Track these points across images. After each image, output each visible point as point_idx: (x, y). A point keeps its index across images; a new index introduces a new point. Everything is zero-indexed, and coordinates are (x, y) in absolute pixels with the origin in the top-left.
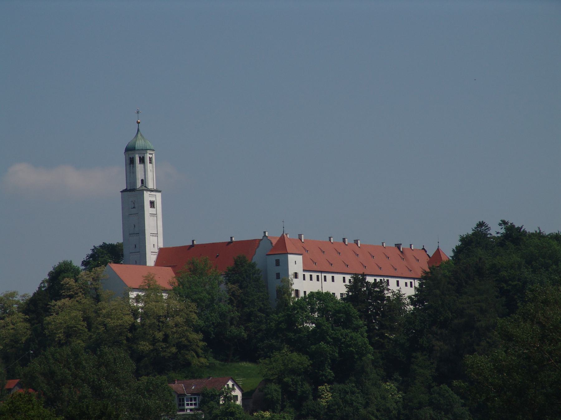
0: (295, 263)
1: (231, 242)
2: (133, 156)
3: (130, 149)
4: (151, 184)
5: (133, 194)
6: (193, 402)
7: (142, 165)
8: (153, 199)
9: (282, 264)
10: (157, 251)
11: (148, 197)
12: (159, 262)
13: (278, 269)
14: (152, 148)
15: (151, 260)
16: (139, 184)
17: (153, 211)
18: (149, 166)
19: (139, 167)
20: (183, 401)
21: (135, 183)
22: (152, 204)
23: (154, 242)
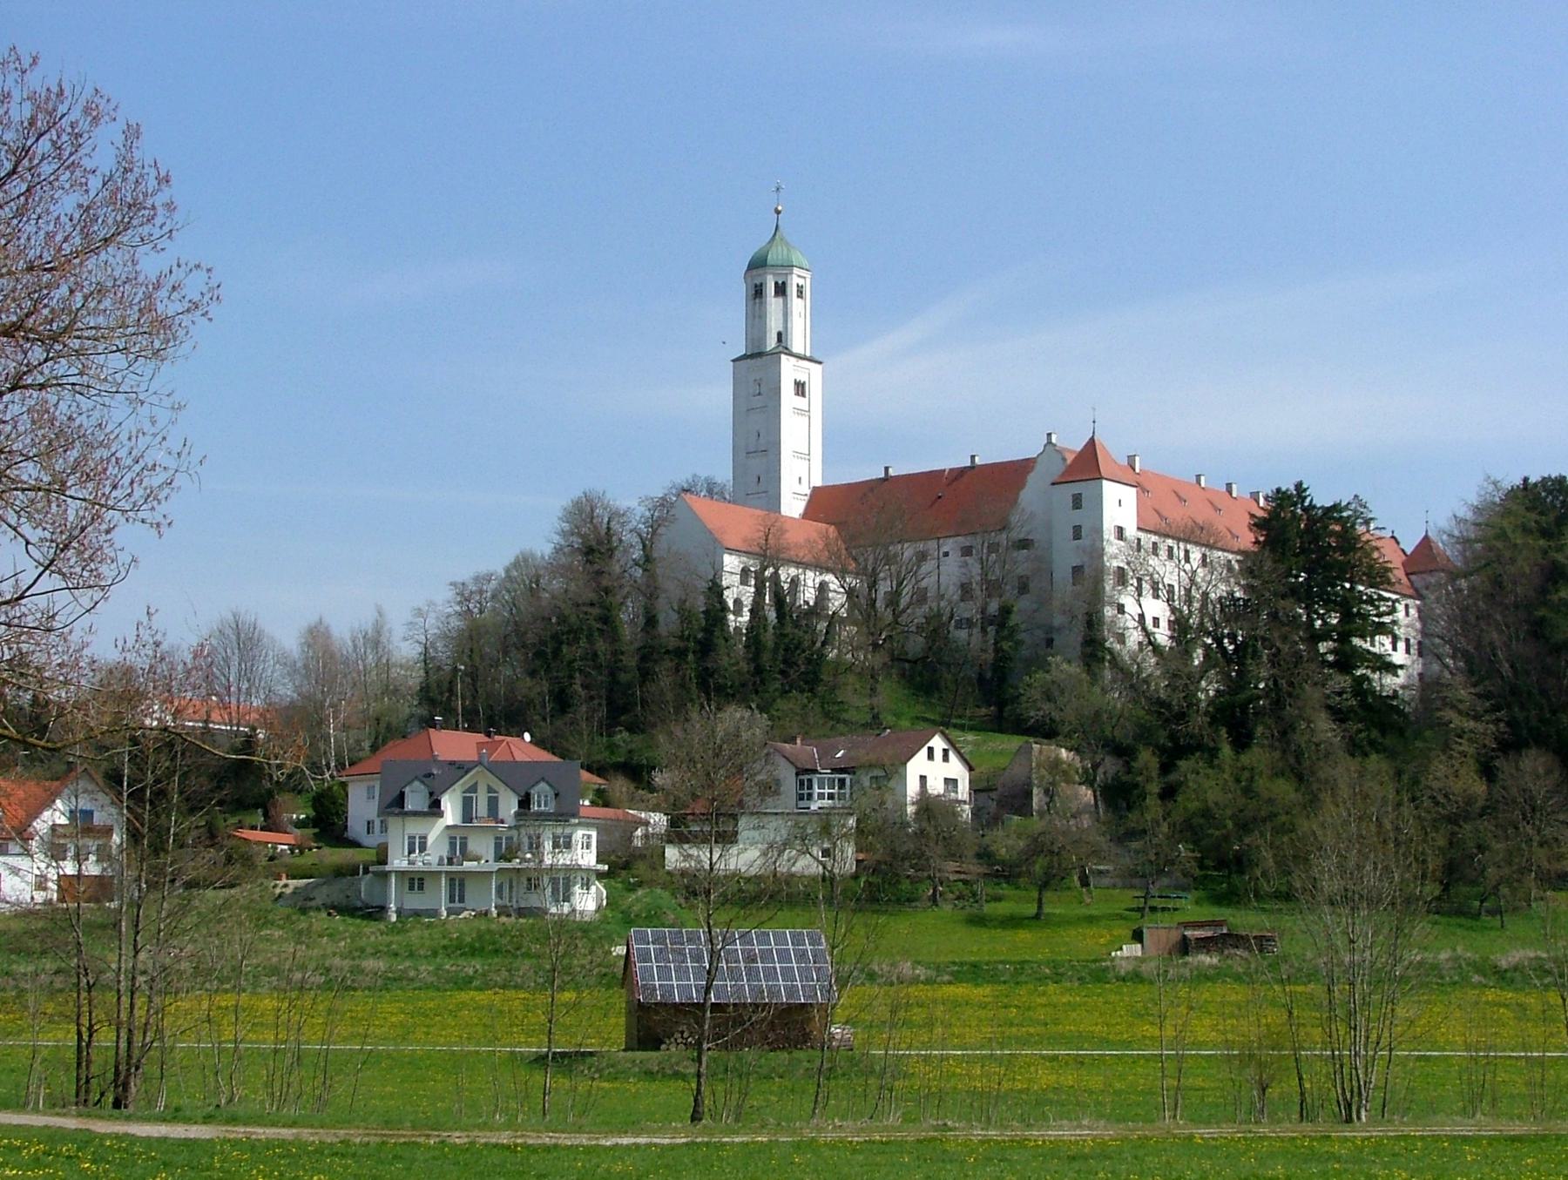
0: (1119, 506)
1: (973, 467)
2: (762, 279)
3: (758, 264)
4: (798, 343)
5: (758, 362)
6: (827, 791)
7: (780, 300)
8: (802, 378)
9: (1086, 504)
10: (808, 492)
11: (789, 370)
12: (811, 512)
13: (1077, 517)
14: (805, 264)
15: (793, 505)
16: (771, 343)
17: (801, 402)
18: (797, 305)
19: (773, 303)
20: (810, 787)
21: (762, 338)
22: (800, 388)
23: (801, 473)
